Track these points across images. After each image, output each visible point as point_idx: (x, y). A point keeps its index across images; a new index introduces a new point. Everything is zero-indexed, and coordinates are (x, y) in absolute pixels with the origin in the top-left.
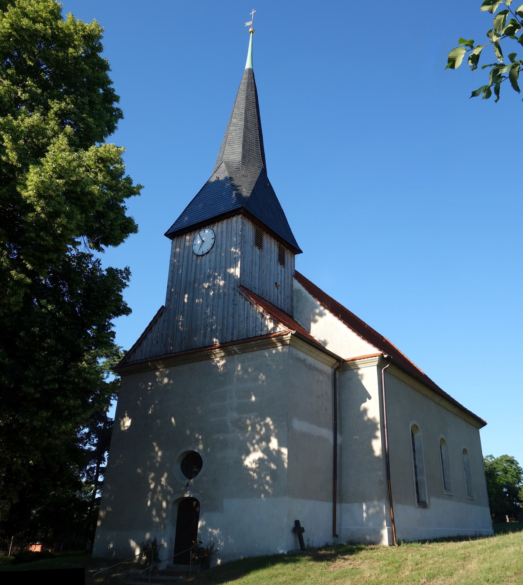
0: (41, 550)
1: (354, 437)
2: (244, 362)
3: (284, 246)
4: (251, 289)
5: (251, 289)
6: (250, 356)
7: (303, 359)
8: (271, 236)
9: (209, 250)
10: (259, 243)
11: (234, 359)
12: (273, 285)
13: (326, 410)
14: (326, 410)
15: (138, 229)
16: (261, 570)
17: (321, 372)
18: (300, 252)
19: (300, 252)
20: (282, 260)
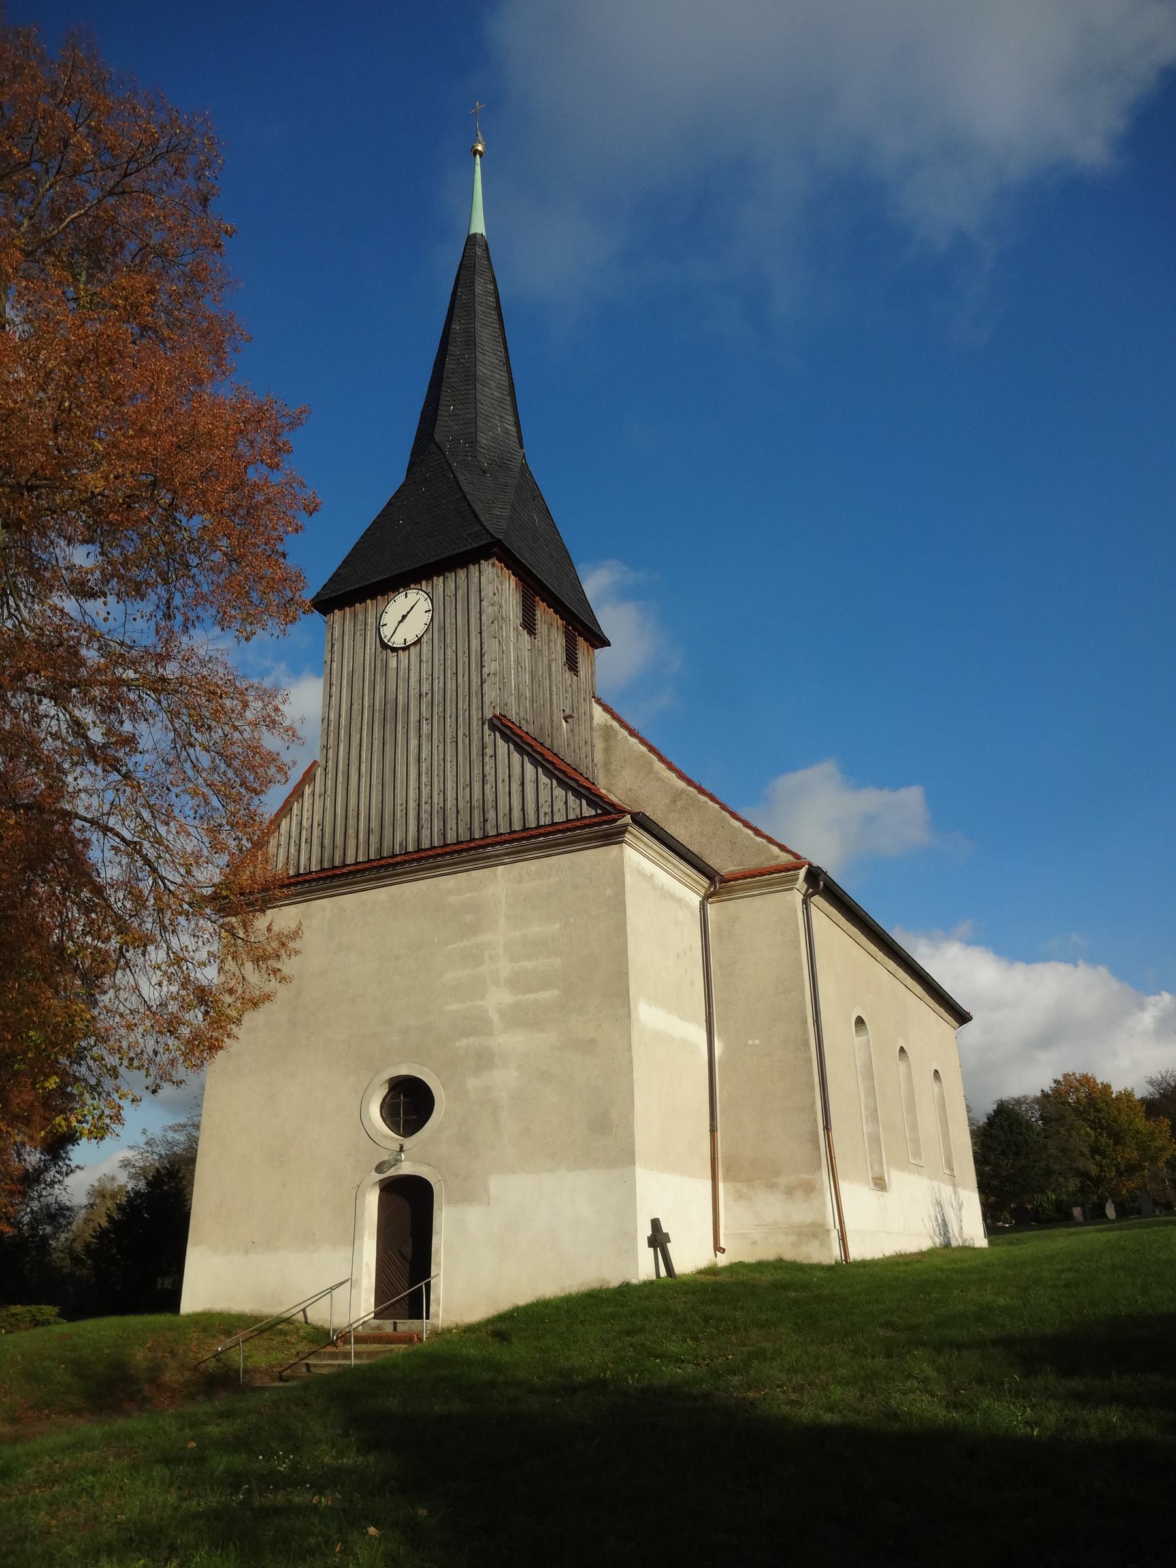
0: (1152, 1107)
1: (750, 1042)
2: (520, 882)
3: (575, 629)
4: (520, 722)
5: (520, 722)
6: (533, 868)
7: (649, 874)
8: (373, 597)
9: (419, 636)
10: (529, 625)
11: (497, 875)
12: (558, 716)
13: (692, 984)
14: (692, 984)
15: (379, 597)
16: (574, 1294)
17: (680, 902)
18: (605, 643)
19: (605, 643)
20: (572, 664)
